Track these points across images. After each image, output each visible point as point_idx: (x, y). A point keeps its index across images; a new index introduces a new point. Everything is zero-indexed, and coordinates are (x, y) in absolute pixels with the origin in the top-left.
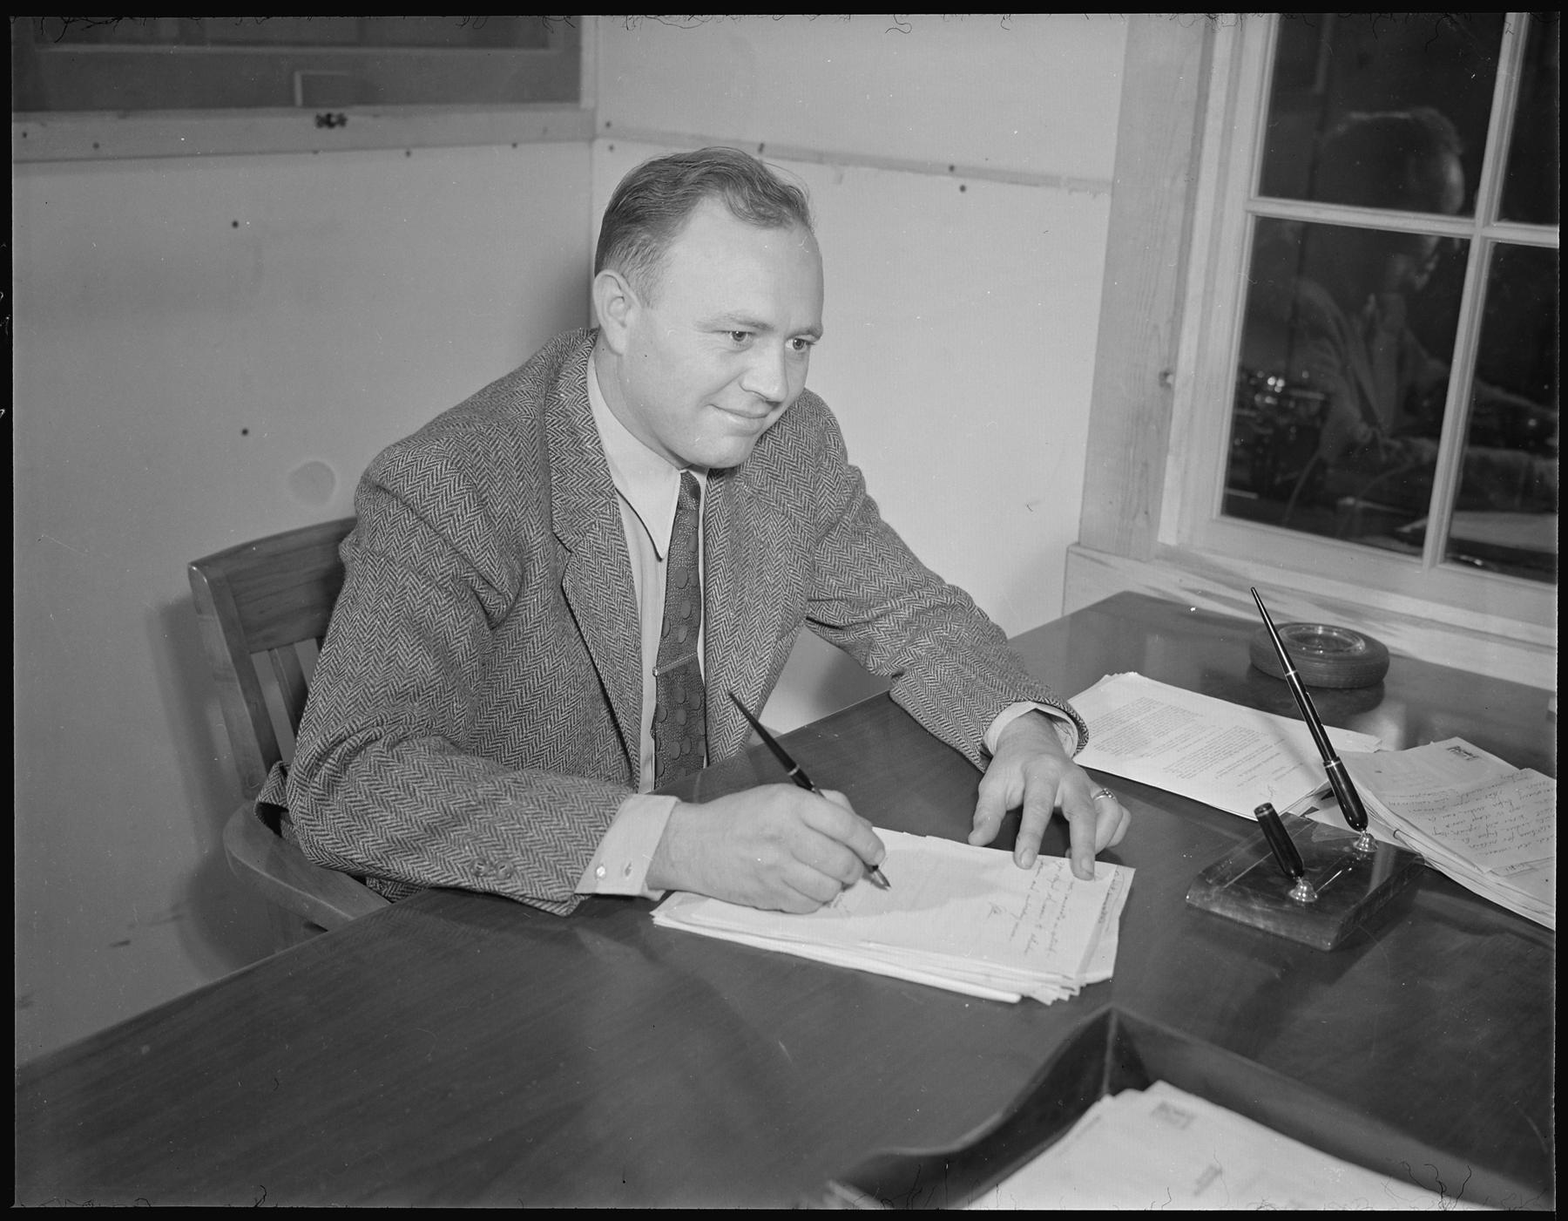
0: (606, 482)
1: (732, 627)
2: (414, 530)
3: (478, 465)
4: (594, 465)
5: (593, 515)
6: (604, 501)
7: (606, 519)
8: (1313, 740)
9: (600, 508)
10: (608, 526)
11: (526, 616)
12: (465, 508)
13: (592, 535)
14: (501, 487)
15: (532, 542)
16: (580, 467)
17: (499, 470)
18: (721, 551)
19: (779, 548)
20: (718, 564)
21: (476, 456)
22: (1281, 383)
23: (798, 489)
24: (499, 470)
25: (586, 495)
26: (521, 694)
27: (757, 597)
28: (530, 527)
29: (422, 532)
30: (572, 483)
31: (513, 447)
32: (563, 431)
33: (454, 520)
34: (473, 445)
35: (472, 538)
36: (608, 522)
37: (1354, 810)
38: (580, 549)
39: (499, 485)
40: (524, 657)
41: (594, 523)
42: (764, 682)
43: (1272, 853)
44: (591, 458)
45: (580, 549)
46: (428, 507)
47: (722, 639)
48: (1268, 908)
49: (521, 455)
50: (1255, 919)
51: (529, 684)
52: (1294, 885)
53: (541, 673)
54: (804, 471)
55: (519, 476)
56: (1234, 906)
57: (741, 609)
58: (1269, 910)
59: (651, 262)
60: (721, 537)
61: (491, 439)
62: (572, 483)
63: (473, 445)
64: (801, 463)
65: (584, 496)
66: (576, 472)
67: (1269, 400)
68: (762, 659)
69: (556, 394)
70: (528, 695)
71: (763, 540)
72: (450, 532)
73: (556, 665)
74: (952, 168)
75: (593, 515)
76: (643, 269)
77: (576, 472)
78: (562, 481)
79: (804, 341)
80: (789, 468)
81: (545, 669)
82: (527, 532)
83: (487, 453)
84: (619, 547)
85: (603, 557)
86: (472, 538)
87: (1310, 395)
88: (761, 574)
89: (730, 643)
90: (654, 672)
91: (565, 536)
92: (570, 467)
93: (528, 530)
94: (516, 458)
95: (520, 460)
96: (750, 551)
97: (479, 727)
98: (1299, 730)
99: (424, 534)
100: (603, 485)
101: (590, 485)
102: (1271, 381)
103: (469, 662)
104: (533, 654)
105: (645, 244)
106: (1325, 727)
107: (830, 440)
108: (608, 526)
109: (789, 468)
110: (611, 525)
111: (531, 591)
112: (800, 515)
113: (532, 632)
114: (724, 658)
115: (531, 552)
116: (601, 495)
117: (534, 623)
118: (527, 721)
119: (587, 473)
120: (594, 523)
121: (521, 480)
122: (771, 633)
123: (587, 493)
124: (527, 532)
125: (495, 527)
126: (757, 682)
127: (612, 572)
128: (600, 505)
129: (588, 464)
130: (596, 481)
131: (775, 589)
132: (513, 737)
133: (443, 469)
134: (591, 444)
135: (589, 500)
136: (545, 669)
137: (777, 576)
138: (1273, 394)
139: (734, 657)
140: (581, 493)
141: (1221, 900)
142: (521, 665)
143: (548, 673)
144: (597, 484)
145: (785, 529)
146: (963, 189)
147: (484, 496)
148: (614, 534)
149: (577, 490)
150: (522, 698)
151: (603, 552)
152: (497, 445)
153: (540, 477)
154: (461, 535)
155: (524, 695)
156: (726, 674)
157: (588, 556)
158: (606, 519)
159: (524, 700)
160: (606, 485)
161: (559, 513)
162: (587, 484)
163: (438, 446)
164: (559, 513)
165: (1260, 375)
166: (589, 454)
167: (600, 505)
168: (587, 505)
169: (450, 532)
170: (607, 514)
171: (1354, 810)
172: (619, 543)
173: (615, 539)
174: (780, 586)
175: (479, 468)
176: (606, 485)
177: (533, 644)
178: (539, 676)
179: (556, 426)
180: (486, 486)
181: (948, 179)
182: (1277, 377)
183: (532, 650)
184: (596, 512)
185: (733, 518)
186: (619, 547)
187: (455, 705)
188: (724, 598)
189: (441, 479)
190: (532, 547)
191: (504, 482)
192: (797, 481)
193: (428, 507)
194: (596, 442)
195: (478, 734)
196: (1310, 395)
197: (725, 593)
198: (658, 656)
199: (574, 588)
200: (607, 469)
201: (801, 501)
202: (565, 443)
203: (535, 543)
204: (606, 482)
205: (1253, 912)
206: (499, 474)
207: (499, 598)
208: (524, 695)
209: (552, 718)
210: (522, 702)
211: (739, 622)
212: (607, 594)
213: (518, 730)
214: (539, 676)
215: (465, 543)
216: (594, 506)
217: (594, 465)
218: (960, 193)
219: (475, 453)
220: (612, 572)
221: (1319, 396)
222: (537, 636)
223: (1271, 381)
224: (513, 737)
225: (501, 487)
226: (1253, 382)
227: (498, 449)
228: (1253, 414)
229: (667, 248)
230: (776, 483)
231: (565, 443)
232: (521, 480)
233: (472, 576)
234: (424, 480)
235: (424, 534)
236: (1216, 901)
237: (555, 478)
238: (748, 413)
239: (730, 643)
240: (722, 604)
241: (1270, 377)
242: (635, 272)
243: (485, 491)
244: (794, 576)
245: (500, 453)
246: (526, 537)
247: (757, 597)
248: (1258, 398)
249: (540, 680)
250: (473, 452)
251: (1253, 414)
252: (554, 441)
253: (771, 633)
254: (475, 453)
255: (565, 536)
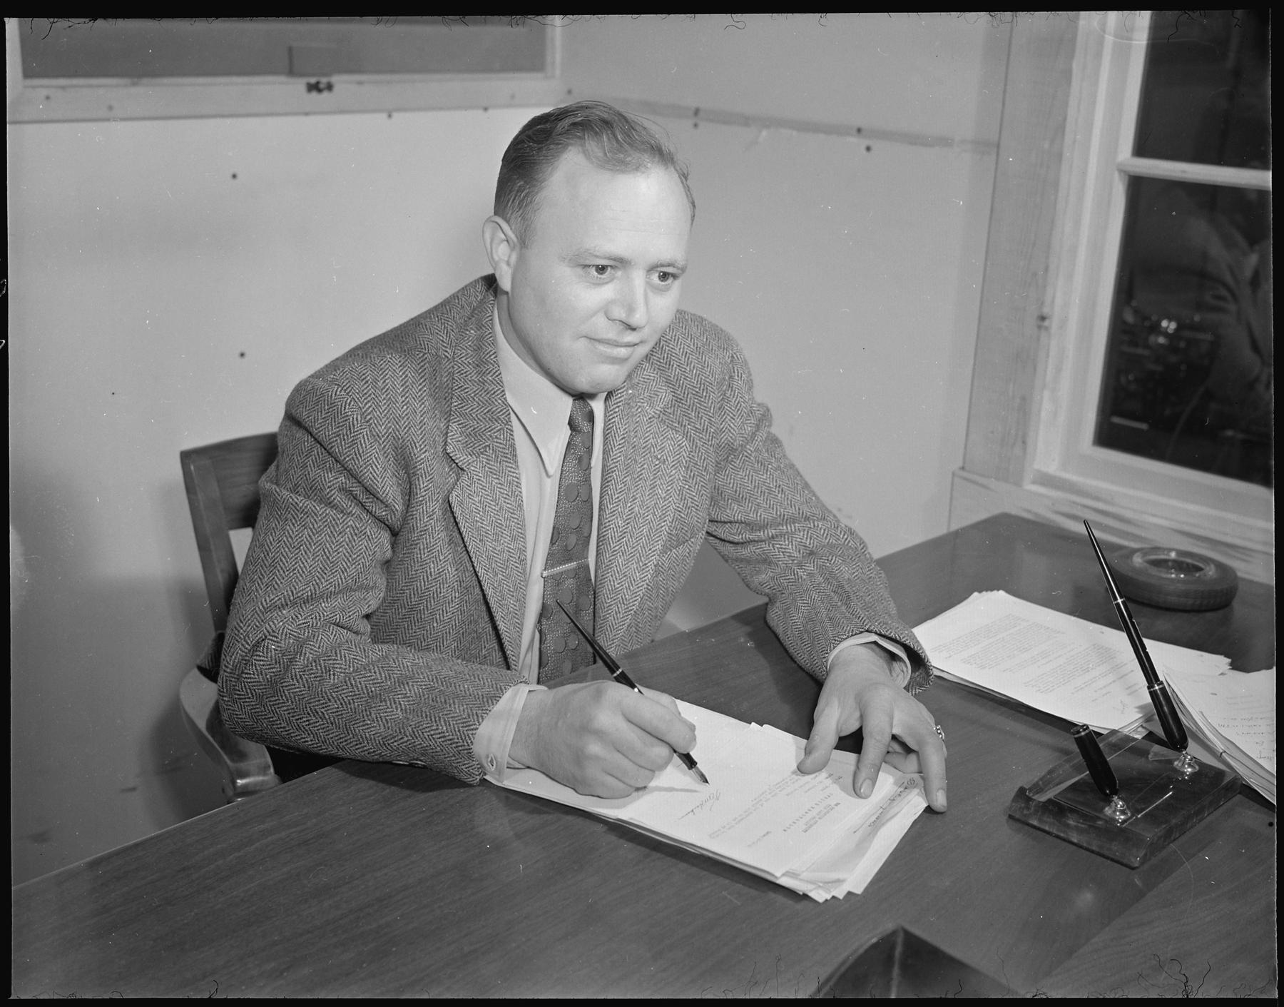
0: (502, 410)
1: (620, 534)
2: (310, 451)
3: (365, 391)
4: (493, 394)
5: (489, 439)
6: (499, 428)
7: (499, 443)
8: (1010, 696)
9: (495, 433)
10: (501, 450)
11: (413, 525)
12: (350, 429)
13: (484, 456)
14: (385, 410)
15: (416, 458)
16: (481, 395)
17: (385, 396)
18: (614, 465)
19: (674, 465)
20: (611, 477)
21: (365, 383)
22: (1173, 326)
23: (699, 413)
24: (385, 396)
25: (483, 420)
26: (410, 595)
27: (647, 508)
28: (413, 445)
29: (318, 452)
30: (472, 410)
31: (401, 376)
32: (470, 363)
33: (340, 440)
34: (364, 374)
35: (356, 455)
36: (501, 446)
37: (1175, 731)
38: (473, 468)
39: (383, 408)
40: (412, 562)
41: (489, 446)
42: (646, 586)
43: (1088, 772)
44: (490, 389)
45: (473, 468)
46: (321, 429)
47: (610, 544)
48: (1082, 823)
49: (407, 384)
50: (1070, 833)
51: (417, 587)
52: (1108, 801)
53: (427, 576)
54: (706, 396)
55: (403, 401)
56: (1051, 820)
57: (630, 518)
58: (1083, 826)
59: (526, 206)
60: (615, 453)
61: (381, 369)
62: (472, 410)
63: (364, 374)
64: (703, 390)
65: (481, 421)
66: (477, 400)
67: (1161, 340)
68: (646, 564)
69: (467, 330)
70: (416, 596)
71: (659, 457)
72: (337, 450)
73: (441, 570)
74: (859, 130)
75: (489, 439)
76: (520, 212)
77: (477, 400)
78: (462, 407)
79: (668, 274)
80: (692, 393)
81: (431, 573)
82: (411, 450)
83: (376, 381)
84: (509, 469)
85: (495, 476)
86: (356, 455)
87: (1201, 336)
88: (654, 487)
89: (617, 548)
90: (542, 574)
91: (458, 456)
92: (472, 395)
93: (412, 448)
94: (402, 386)
95: (406, 388)
96: (645, 466)
97: (377, 619)
98: (1118, 640)
99: (318, 454)
100: (499, 412)
101: (488, 412)
102: (1164, 324)
103: (354, 566)
104: (420, 559)
105: (520, 190)
106: (1146, 641)
107: (734, 372)
108: (501, 450)
109: (692, 393)
110: (503, 448)
111: (417, 503)
112: (699, 436)
113: (419, 540)
114: (610, 561)
115: (416, 467)
116: (497, 421)
117: (421, 531)
118: (416, 619)
119: (487, 401)
120: (489, 446)
121: (406, 405)
122: (656, 542)
123: (485, 419)
124: (411, 450)
125: (380, 445)
126: (640, 585)
127: (502, 491)
128: (495, 430)
129: (488, 393)
130: (494, 409)
131: (666, 502)
132: (403, 632)
133: (333, 395)
134: (492, 376)
135: (486, 426)
136: (431, 573)
137: (668, 490)
138: (1166, 334)
139: (620, 561)
140: (479, 419)
141: (1039, 813)
142: (410, 569)
143: (434, 577)
144: (494, 411)
145: (681, 448)
146: (868, 149)
147: (369, 417)
148: (506, 457)
149: (476, 415)
150: (410, 598)
151: (495, 472)
152: (387, 374)
153: (427, 403)
154: (346, 453)
155: (412, 596)
156: (612, 576)
157: (480, 475)
158: (499, 443)
159: (413, 600)
160: (501, 413)
161: (454, 435)
162: (485, 411)
163: (334, 375)
164: (454, 435)
165: (1154, 318)
166: (489, 385)
167: (495, 430)
168: (484, 429)
169: (337, 450)
170: (500, 439)
171: (1175, 731)
172: (511, 465)
173: (507, 462)
174: (670, 499)
175: (366, 394)
176: (501, 413)
177: (420, 550)
178: (426, 579)
179: (463, 359)
180: (371, 409)
181: (853, 140)
182: (1170, 320)
183: (419, 556)
184: (491, 436)
185: (629, 436)
186: (509, 469)
187: (323, 605)
188: (614, 507)
189: (331, 404)
190: (416, 463)
191: (388, 405)
192: (698, 405)
193: (321, 429)
194: (497, 374)
195: (376, 626)
196: (1201, 336)
197: (615, 502)
198: (547, 560)
199: (461, 503)
200: (504, 399)
201: (701, 424)
202: (470, 374)
203: (418, 459)
204: (502, 410)
205: (1068, 826)
206: (384, 399)
207: (386, 511)
208: (412, 596)
209: (438, 617)
210: (411, 602)
211: (628, 530)
212: (495, 510)
213: (408, 626)
214: (426, 579)
215: (350, 460)
216: (489, 431)
217: (493, 394)
218: (864, 152)
219: (364, 382)
220: (502, 491)
221: (1208, 337)
222: (423, 543)
223: (1164, 324)
224: (403, 632)
225: (385, 410)
226: (1147, 324)
227: (387, 377)
228: (1146, 352)
229: (537, 193)
230: (679, 406)
231: (470, 374)
232: (406, 405)
233: (357, 491)
234: (318, 405)
235: (318, 454)
236: (1034, 814)
237: (455, 404)
238: (615, 341)
239: (617, 548)
240: (611, 513)
241: (1164, 319)
242: (514, 216)
243: (369, 414)
244: (688, 491)
245: (387, 381)
246: (410, 453)
247: (647, 508)
248: (1152, 339)
249: (427, 583)
250: (363, 380)
251: (1146, 352)
252: (459, 372)
253: (656, 542)
254: (364, 382)
255: (458, 456)
